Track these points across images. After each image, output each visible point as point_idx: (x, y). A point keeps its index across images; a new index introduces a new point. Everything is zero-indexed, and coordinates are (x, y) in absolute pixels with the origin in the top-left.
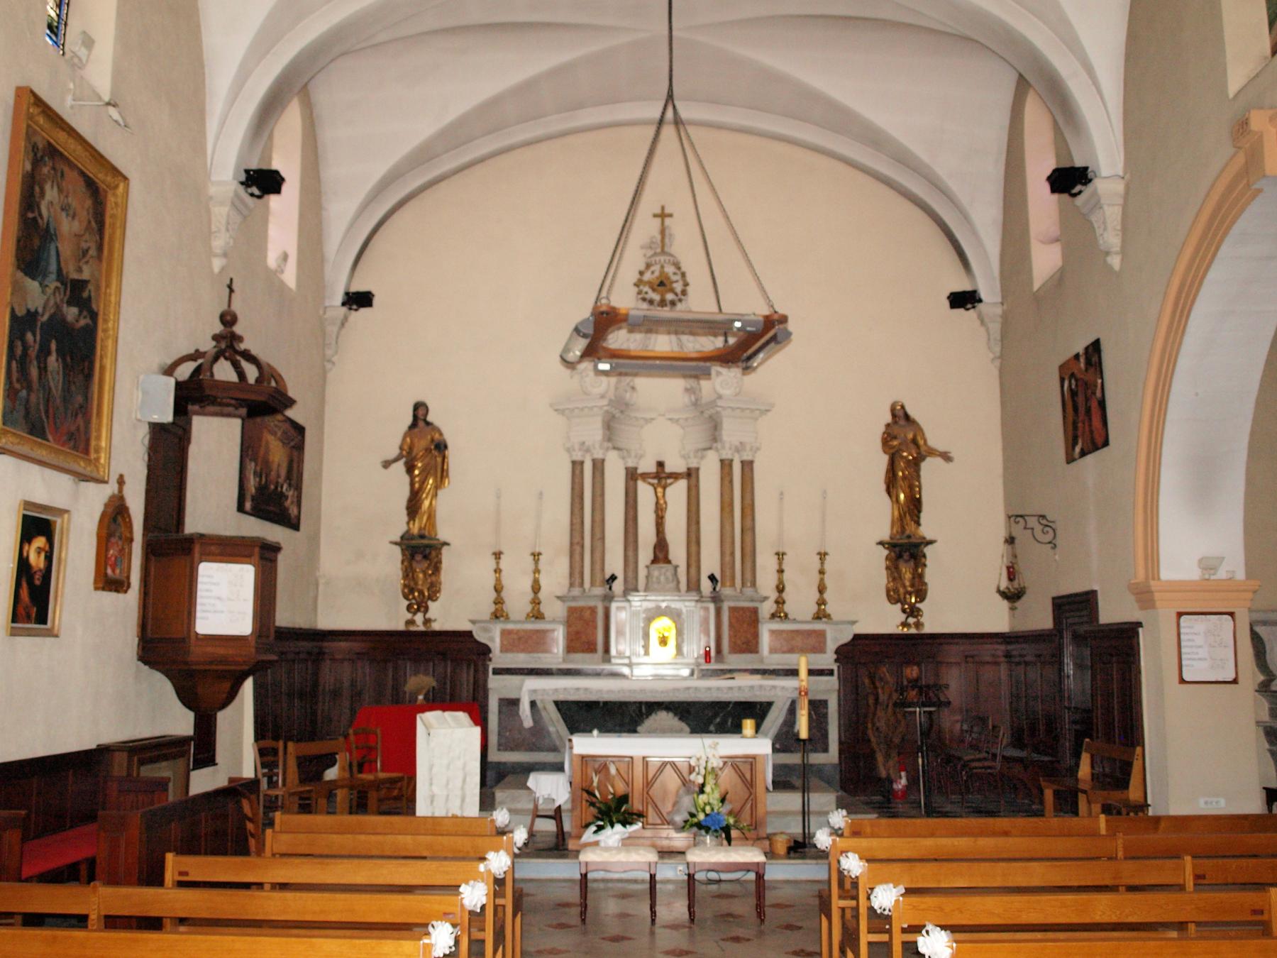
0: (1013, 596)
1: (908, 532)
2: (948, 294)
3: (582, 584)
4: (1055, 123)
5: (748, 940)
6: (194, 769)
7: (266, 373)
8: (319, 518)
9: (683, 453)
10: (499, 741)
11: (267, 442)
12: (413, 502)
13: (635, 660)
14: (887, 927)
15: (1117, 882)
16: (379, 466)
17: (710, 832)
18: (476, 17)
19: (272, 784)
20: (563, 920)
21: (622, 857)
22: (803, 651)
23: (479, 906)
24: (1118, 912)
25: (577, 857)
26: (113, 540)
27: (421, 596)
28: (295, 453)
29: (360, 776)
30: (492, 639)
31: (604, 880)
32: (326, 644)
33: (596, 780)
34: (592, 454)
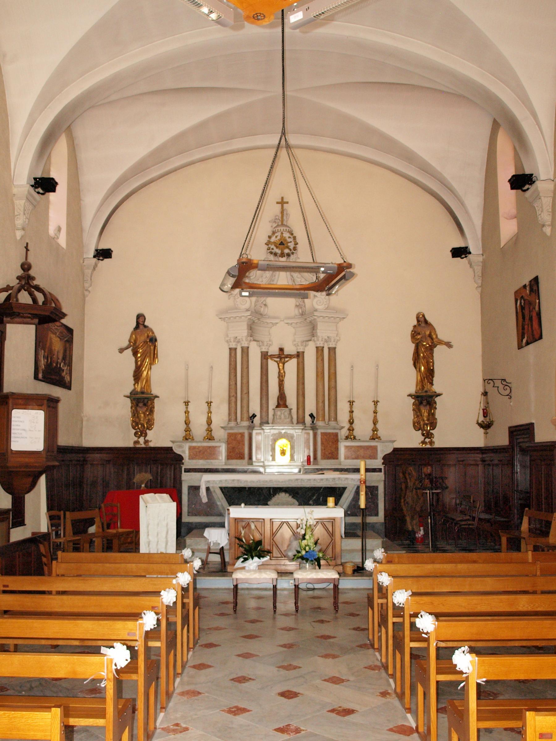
0: (486, 426)
1: (426, 389)
2: (451, 249)
3: (236, 419)
4: (515, 149)
5: (329, 622)
6: (11, 528)
7: (49, 298)
8: (82, 382)
9: (295, 343)
10: (188, 511)
11: (51, 339)
12: (137, 373)
13: (266, 463)
14: (402, 613)
15: (534, 589)
17: (309, 561)
18: (169, 84)
19: (58, 535)
20: (223, 611)
21: (257, 576)
22: (364, 458)
23: (172, 603)
24: (532, 605)
25: (231, 576)
27: (143, 427)
28: (68, 345)
29: (110, 531)
30: (184, 452)
31: (248, 589)
32: (88, 455)
33: (243, 532)
34: (241, 344)
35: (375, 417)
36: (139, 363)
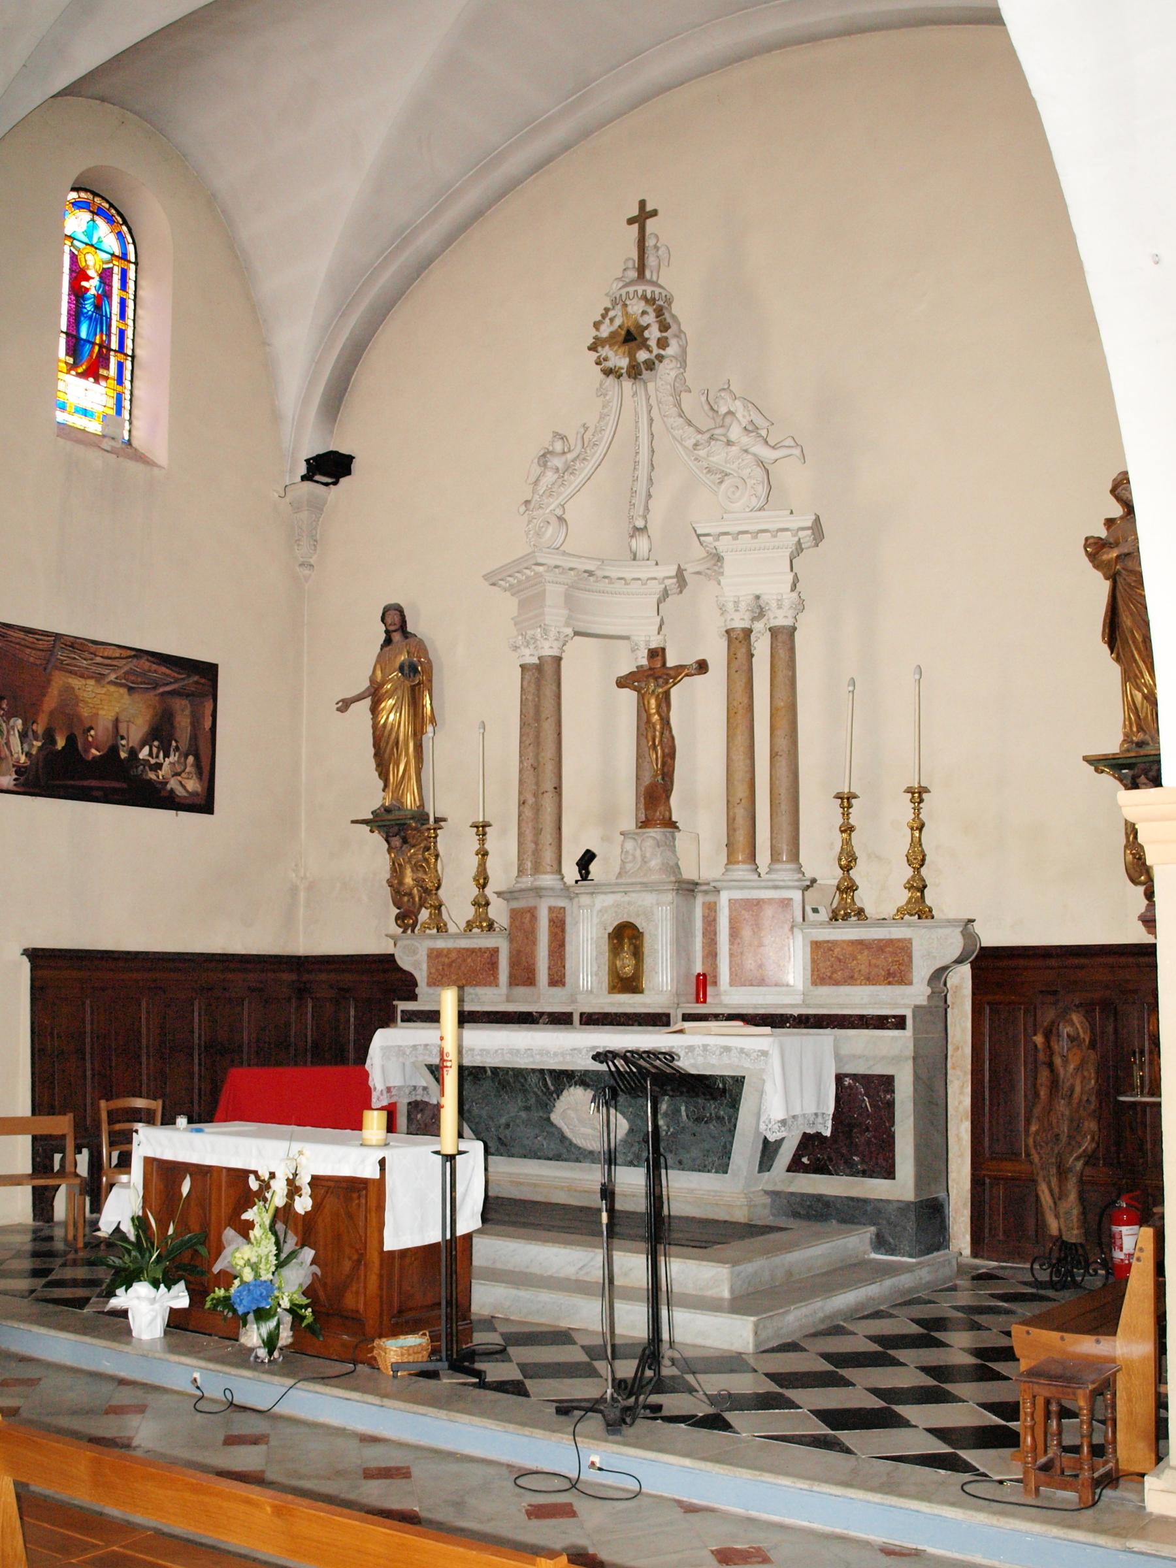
35: (917, 843)
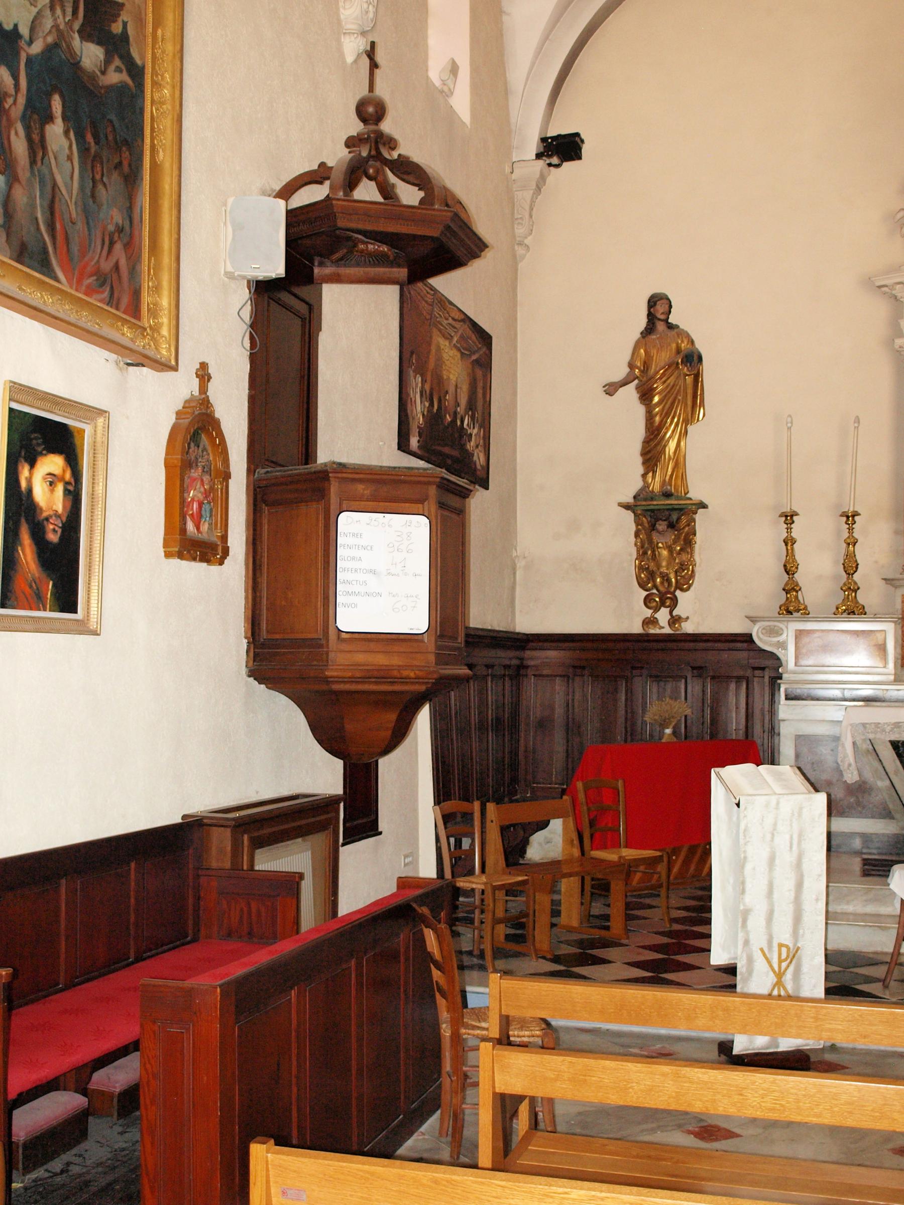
6: (343, 845)
11: (439, 349)
12: (653, 444)
16: (600, 391)
26: (195, 473)
27: (666, 585)
28: (479, 373)
32: (528, 653)
36: (657, 419)
